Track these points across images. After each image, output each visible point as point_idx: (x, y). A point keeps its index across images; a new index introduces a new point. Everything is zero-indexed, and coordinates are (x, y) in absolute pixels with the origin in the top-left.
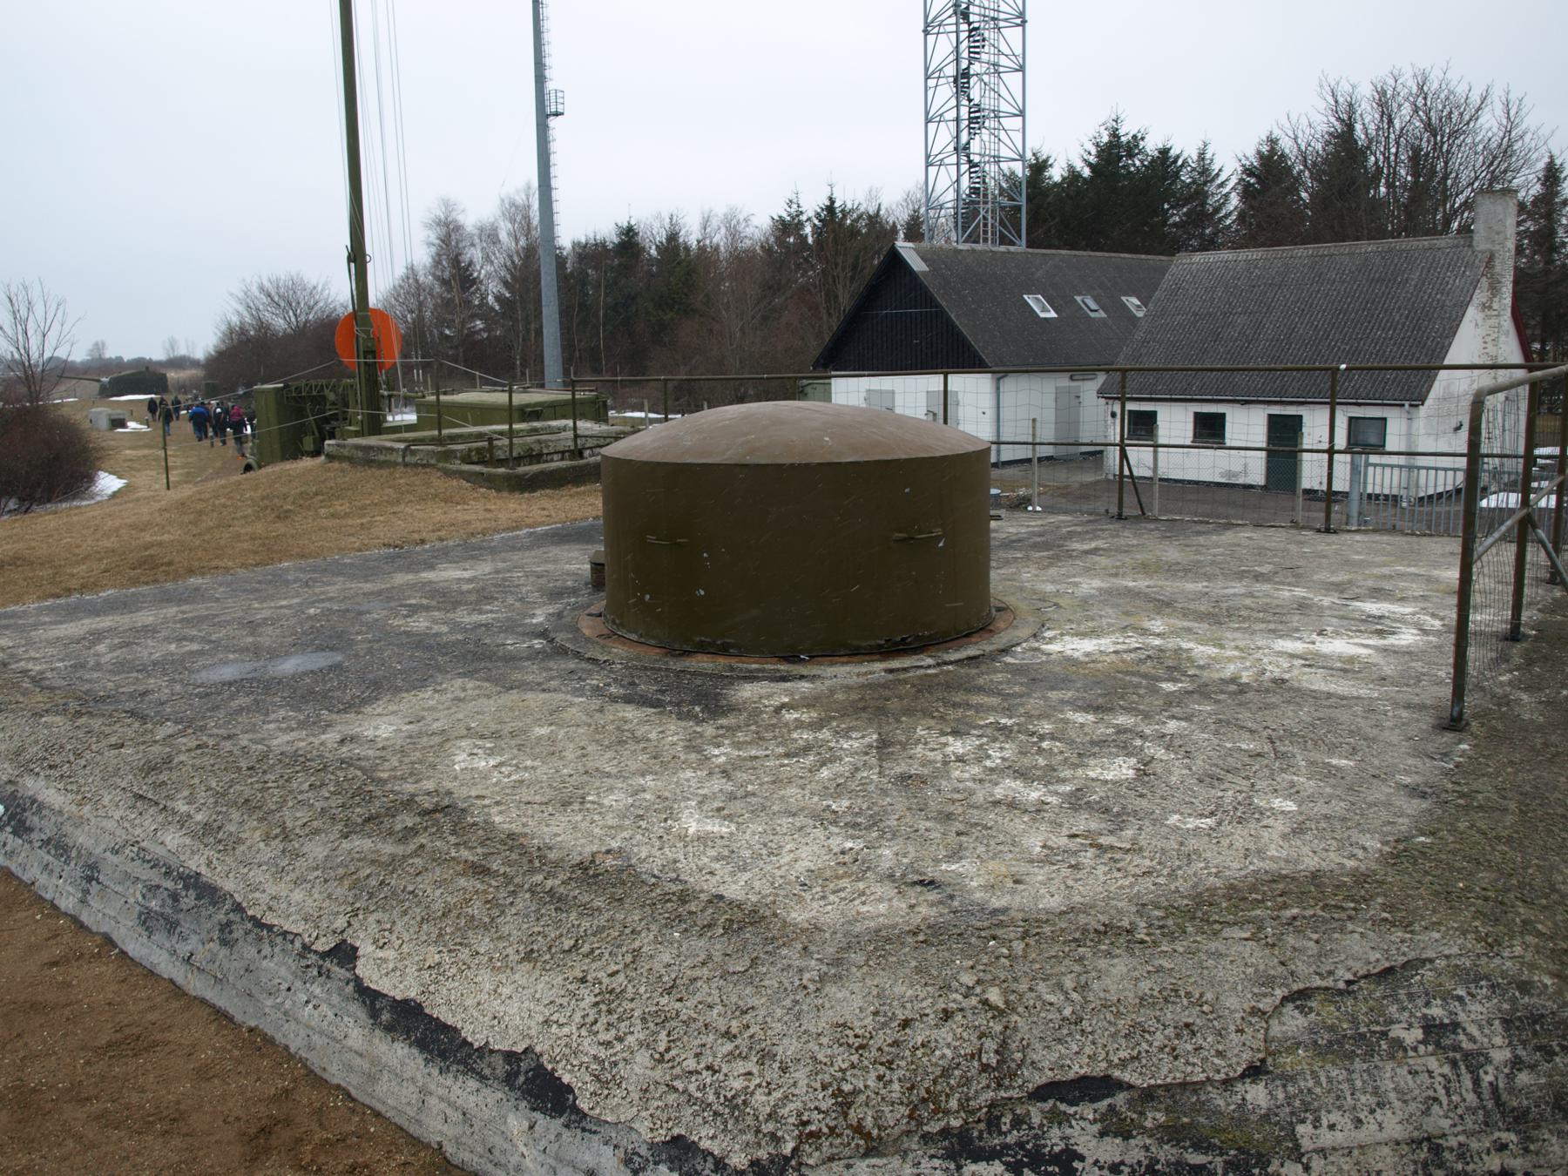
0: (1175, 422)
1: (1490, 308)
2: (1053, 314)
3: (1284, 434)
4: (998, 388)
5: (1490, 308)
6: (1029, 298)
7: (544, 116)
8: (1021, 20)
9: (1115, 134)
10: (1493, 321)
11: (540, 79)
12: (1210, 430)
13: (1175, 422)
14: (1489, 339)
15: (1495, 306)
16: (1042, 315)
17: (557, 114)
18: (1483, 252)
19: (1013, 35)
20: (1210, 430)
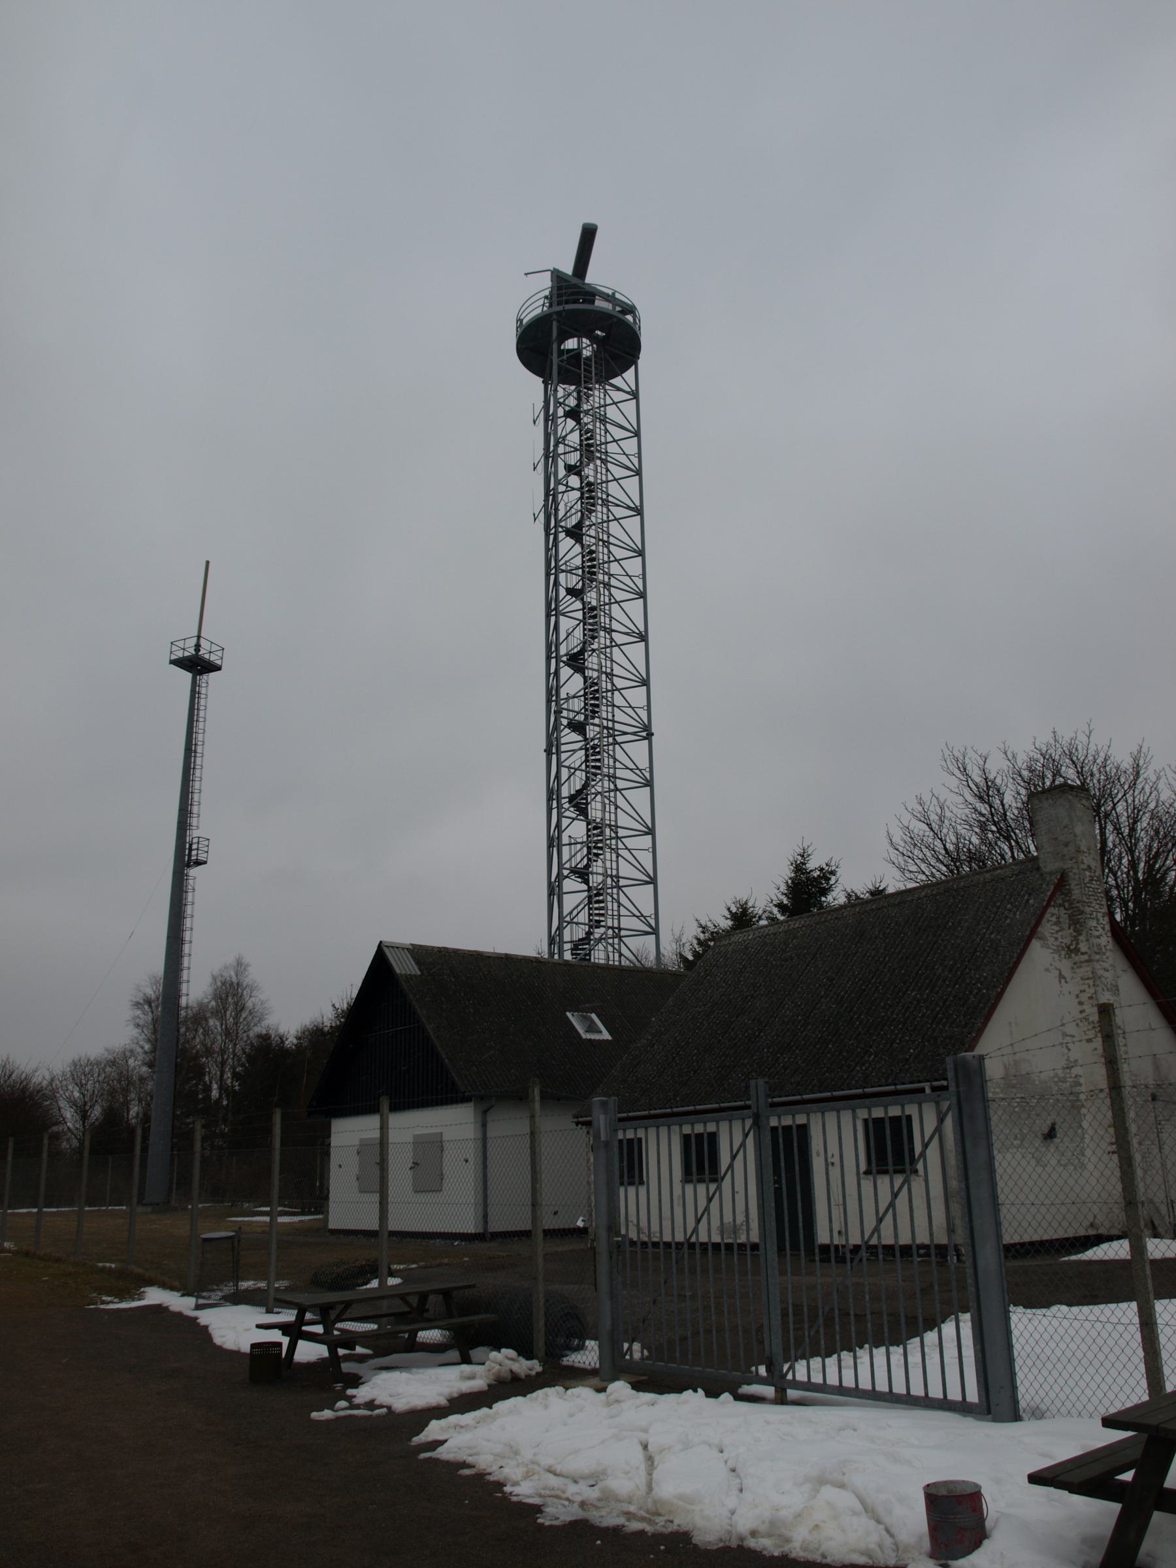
0: (663, 1151)
1: (1077, 951)
2: (606, 1035)
3: (788, 1165)
4: (484, 1125)
5: (1077, 951)
6: (568, 1014)
7: (186, 860)
8: (647, 732)
9: (799, 868)
10: (1085, 970)
11: (183, 825)
12: (701, 1162)
13: (663, 1151)
14: (1084, 997)
15: (1083, 947)
16: (585, 1036)
17: (198, 863)
18: (1051, 873)
19: (638, 751)
20: (701, 1162)
